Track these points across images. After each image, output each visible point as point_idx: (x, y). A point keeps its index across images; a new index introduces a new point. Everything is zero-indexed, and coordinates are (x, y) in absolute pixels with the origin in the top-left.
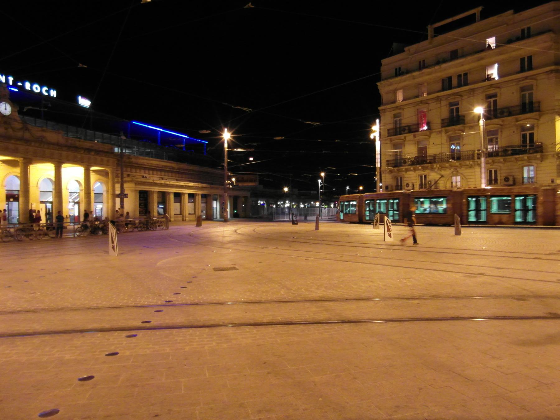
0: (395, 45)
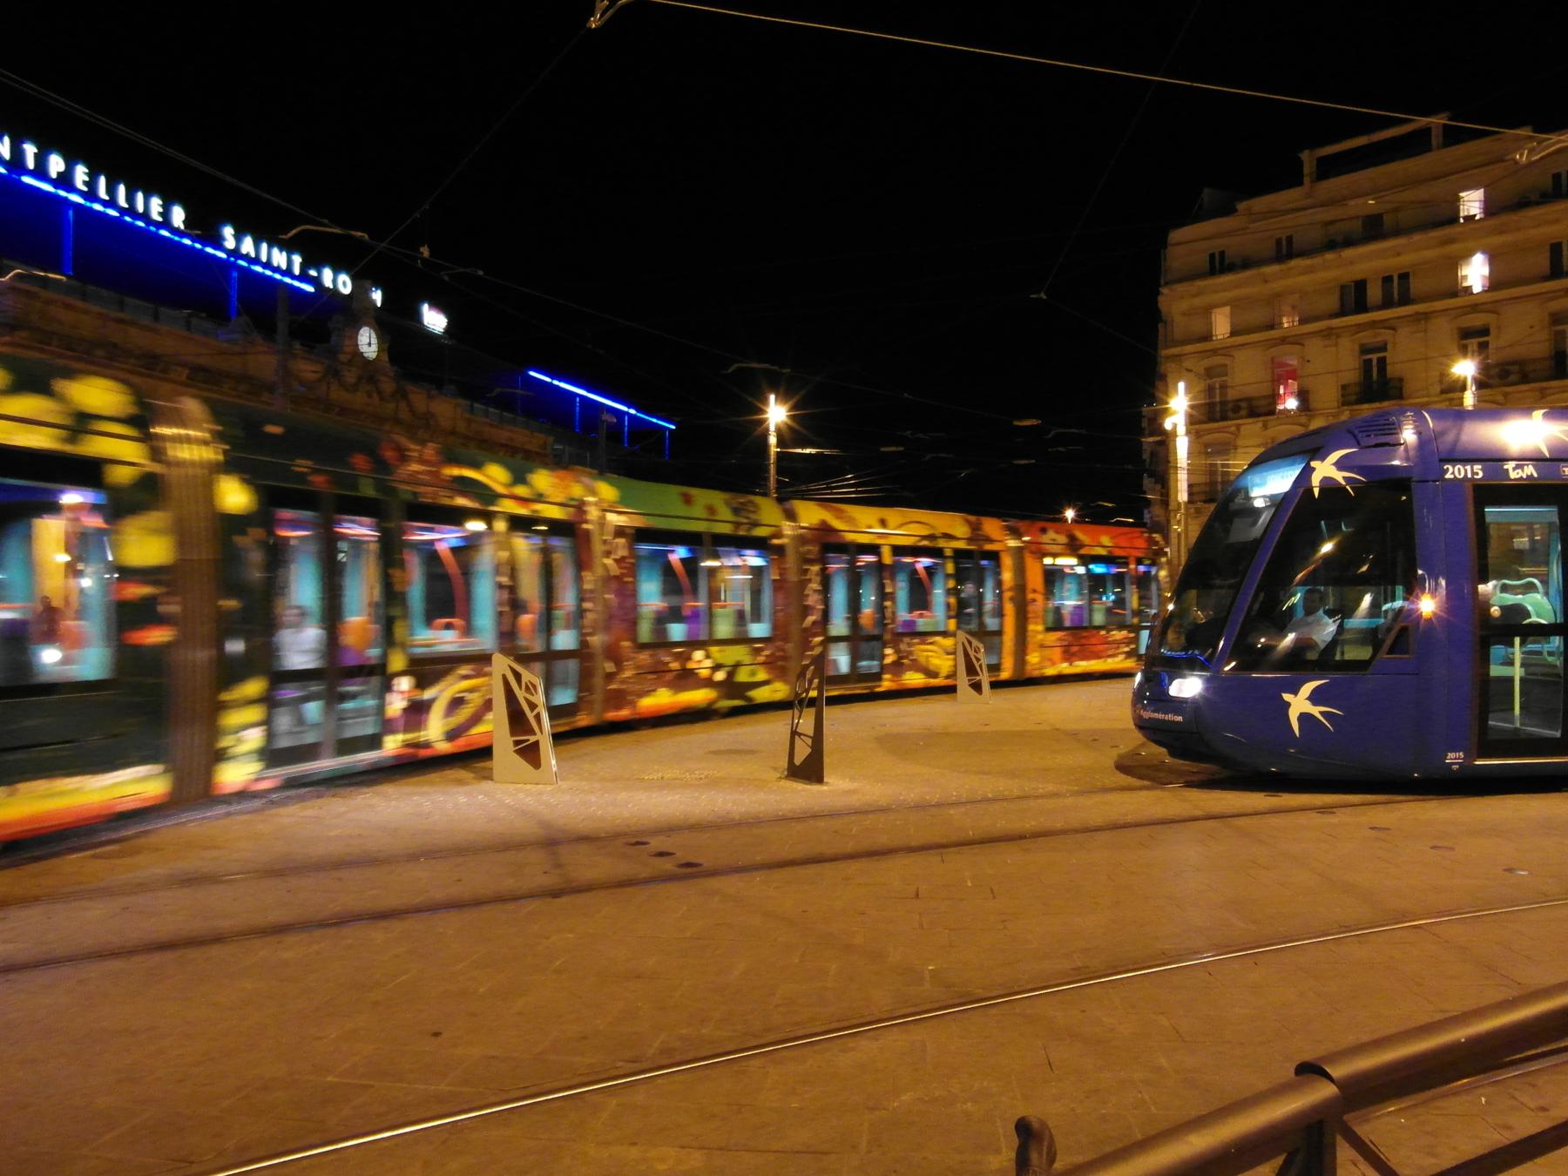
0: (1207, 194)
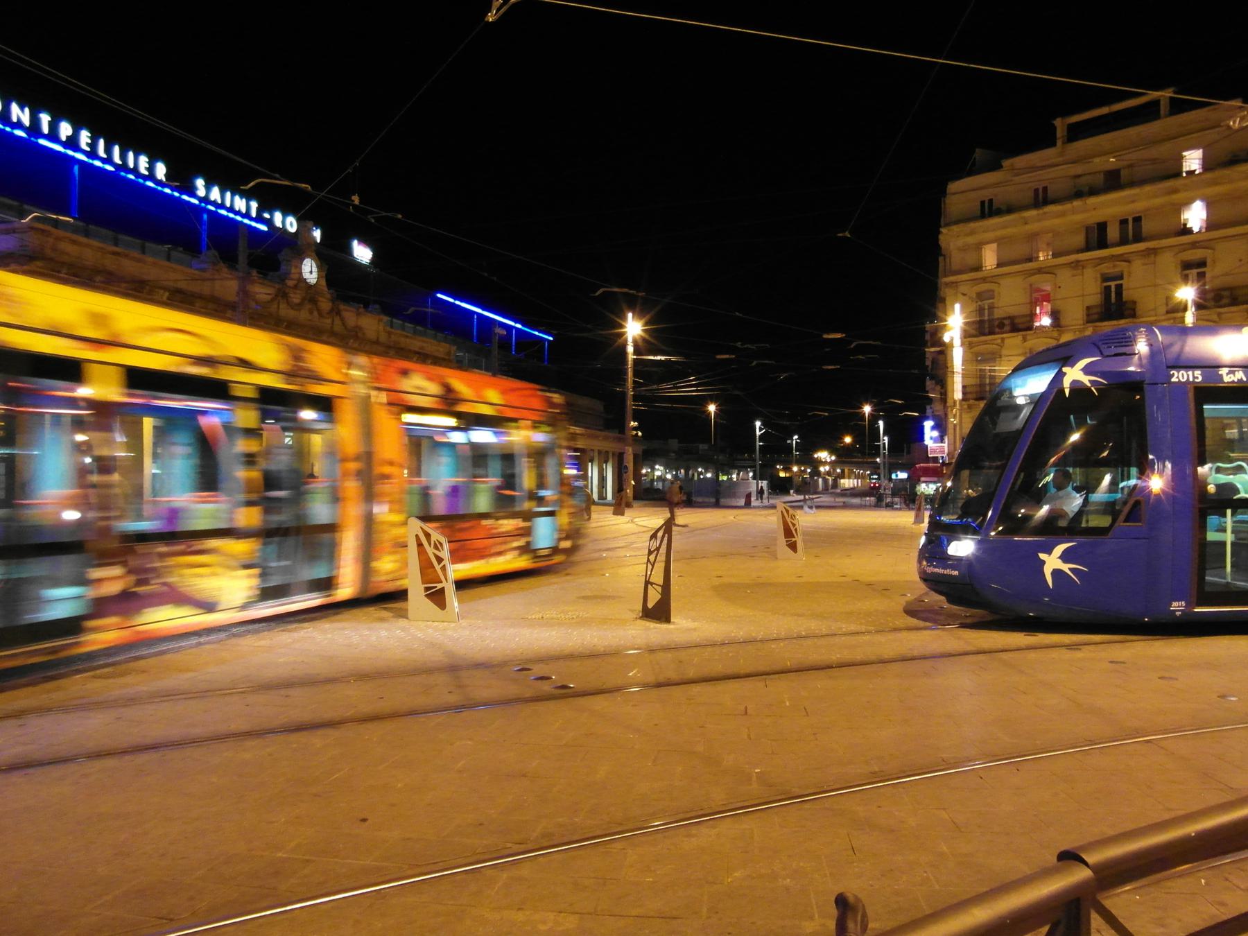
0: (979, 154)
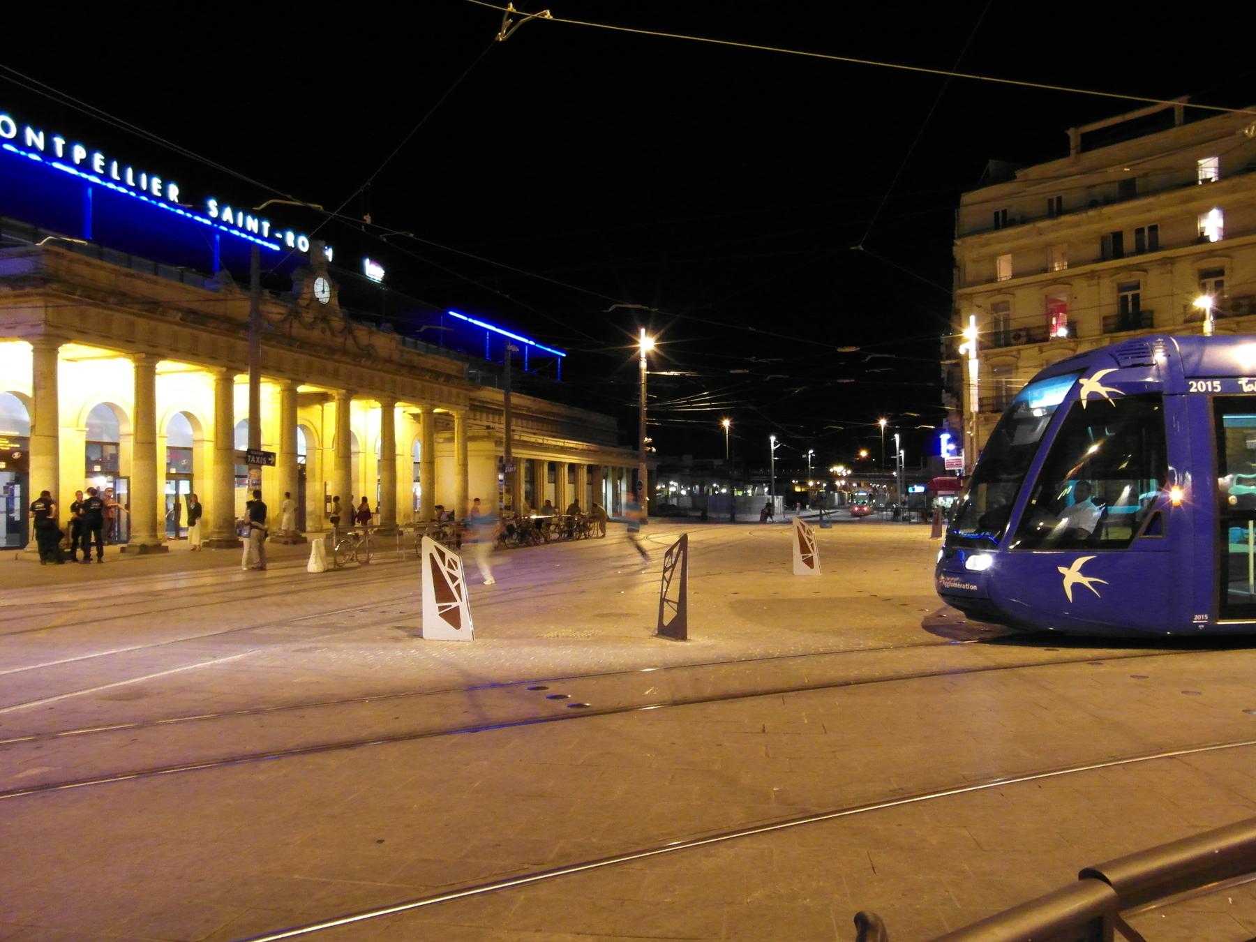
0: (992, 164)
